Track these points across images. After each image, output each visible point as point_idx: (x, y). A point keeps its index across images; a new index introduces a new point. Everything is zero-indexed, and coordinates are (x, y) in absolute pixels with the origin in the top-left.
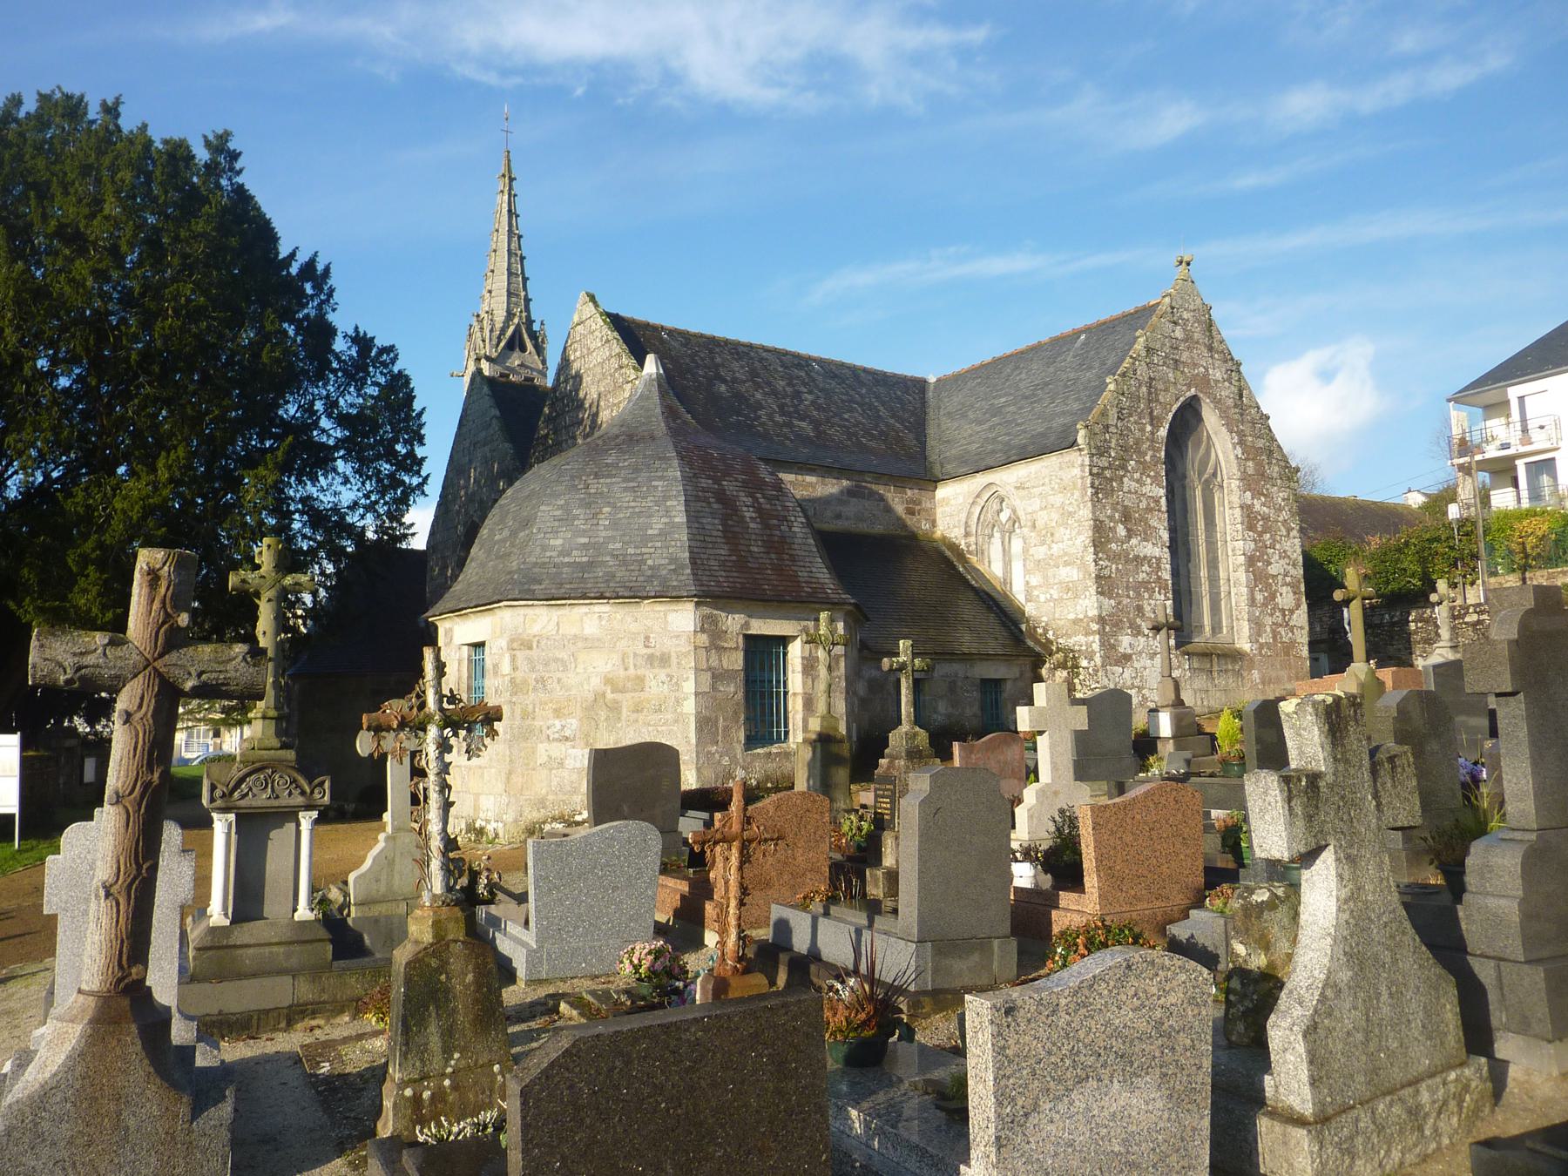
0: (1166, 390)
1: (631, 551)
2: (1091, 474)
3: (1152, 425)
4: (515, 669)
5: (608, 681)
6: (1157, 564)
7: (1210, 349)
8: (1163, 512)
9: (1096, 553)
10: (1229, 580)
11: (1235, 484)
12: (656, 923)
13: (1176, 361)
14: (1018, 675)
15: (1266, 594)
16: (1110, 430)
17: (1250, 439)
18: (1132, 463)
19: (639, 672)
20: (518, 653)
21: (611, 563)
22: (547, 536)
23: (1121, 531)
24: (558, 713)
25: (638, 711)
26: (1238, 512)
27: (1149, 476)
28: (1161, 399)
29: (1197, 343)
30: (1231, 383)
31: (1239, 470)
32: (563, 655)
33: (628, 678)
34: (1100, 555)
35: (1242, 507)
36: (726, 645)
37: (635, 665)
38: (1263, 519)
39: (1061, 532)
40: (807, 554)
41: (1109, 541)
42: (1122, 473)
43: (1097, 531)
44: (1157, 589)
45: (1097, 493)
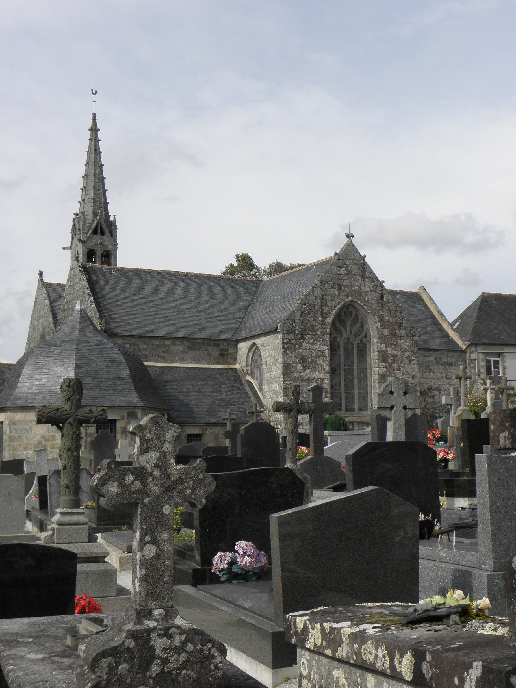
0: (332, 300)
1: (53, 388)
2: (283, 343)
3: (322, 317)
4: (10, 432)
5: (43, 437)
6: (321, 381)
7: (363, 277)
8: (326, 357)
9: (284, 378)
10: (372, 387)
11: (376, 340)
13: (340, 286)
16: (296, 321)
17: (387, 318)
18: (308, 336)
19: (54, 434)
20: (12, 427)
21: (46, 392)
22: (25, 381)
23: (300, 367)
24: (25, 449)
25: (53, 448)
26: (376, 354)
27: (319, 341)
28: (329, 304)
29: (355, 275)
30: (376, 292)
31: (378, 334)
32: (27, 427)
33: (50, 436)
34: (287, 379)
35: (379, 352)
37: (52, 431)
39: (274, 367)
41: (292, 372)
42: (302, 341)
43: (285, 368)
45: (286, 351)
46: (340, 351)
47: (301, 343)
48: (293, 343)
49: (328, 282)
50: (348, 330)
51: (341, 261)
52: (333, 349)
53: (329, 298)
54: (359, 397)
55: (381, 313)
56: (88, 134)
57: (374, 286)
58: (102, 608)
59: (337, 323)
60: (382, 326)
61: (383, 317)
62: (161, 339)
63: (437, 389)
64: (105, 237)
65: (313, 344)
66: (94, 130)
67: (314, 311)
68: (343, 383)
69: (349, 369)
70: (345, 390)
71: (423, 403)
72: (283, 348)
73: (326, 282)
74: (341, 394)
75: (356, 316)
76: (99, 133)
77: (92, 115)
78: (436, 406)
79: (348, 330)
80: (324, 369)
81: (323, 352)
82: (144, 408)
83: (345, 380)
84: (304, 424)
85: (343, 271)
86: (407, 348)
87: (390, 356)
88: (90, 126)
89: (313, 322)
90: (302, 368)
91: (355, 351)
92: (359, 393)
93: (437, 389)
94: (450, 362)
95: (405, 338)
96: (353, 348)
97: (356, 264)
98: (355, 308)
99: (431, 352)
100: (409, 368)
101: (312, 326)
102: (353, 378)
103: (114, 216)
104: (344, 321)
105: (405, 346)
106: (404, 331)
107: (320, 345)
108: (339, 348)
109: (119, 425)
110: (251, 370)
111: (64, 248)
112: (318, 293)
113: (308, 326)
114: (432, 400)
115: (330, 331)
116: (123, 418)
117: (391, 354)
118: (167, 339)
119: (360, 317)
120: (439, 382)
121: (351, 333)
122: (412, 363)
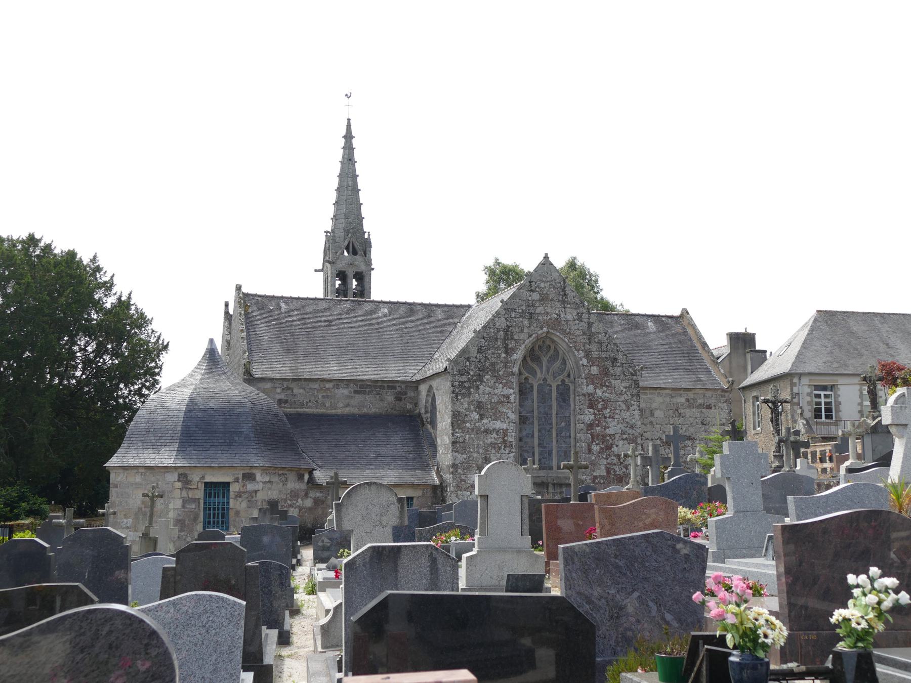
3: (506, 352)
7: (563, 302)
12: (788, 517)
14: (421, 494)
15: (602, 446)
17: (596, 353)
23: (475, 416)
27: (501, 383)
28: (516, 337)
29: (552, 300)
36: (190, 487)
38: (603, 401)
40: (207, 441)
41: (465, 422)
44: (503, 447)
45: (457, 396)
46: (533, 395)
48: (467, 386)
49: (515, 309)
50: (544, 368)
51: (533, 284)
52: (523, 392)
53: (517, 330)
56: (342, 142)
57: (578, 313)
58: (748, 599)
59: (528, 359)
60: (588, 362)
61: (591, 352)
62: (321, 381)
64: (357, 257)
66: (349, 137)
67: (496, 346)
68: (536, 434)
69: (545, 419)
70: (539, 444)
72: (453, 392)
73: (513, 310)
74: (534, 448)
75: (556, 349)
77: (347, 121)
79: (544, 368)
80: (508, 417)
81: (507, 397)
82: (263, 468)
83: (539, 431)
85: (536, 296)
86: (624, 390)
87: (601, 400)
88: (344, 133)
89: (493, 360)
90: (477, 417)
91: (554, 394)
92: (558, 447)
94: (708, 404)
95: (622, 377)
97: (554, 288)
98: (553, 341)
99: (681, 392)
100: (626, 415)
101: (493, 364)
102: (552, 428)
103: (369, 233)
104: (539, 357)
105: (622, 388)
106: (620, 369)
107: (503, 388)
108: (532, 391)
109: (234, 488)
110: (431, 418)
111: (316, 271)
112: (501, 323)
113: (488, 365)
115: (519, 370)
116: (237, 480)
117: (601, 398)
118: (328, 381)
119: (561, 352)
120: (692, 430)
121: (548, 373)
122: (631, 408)
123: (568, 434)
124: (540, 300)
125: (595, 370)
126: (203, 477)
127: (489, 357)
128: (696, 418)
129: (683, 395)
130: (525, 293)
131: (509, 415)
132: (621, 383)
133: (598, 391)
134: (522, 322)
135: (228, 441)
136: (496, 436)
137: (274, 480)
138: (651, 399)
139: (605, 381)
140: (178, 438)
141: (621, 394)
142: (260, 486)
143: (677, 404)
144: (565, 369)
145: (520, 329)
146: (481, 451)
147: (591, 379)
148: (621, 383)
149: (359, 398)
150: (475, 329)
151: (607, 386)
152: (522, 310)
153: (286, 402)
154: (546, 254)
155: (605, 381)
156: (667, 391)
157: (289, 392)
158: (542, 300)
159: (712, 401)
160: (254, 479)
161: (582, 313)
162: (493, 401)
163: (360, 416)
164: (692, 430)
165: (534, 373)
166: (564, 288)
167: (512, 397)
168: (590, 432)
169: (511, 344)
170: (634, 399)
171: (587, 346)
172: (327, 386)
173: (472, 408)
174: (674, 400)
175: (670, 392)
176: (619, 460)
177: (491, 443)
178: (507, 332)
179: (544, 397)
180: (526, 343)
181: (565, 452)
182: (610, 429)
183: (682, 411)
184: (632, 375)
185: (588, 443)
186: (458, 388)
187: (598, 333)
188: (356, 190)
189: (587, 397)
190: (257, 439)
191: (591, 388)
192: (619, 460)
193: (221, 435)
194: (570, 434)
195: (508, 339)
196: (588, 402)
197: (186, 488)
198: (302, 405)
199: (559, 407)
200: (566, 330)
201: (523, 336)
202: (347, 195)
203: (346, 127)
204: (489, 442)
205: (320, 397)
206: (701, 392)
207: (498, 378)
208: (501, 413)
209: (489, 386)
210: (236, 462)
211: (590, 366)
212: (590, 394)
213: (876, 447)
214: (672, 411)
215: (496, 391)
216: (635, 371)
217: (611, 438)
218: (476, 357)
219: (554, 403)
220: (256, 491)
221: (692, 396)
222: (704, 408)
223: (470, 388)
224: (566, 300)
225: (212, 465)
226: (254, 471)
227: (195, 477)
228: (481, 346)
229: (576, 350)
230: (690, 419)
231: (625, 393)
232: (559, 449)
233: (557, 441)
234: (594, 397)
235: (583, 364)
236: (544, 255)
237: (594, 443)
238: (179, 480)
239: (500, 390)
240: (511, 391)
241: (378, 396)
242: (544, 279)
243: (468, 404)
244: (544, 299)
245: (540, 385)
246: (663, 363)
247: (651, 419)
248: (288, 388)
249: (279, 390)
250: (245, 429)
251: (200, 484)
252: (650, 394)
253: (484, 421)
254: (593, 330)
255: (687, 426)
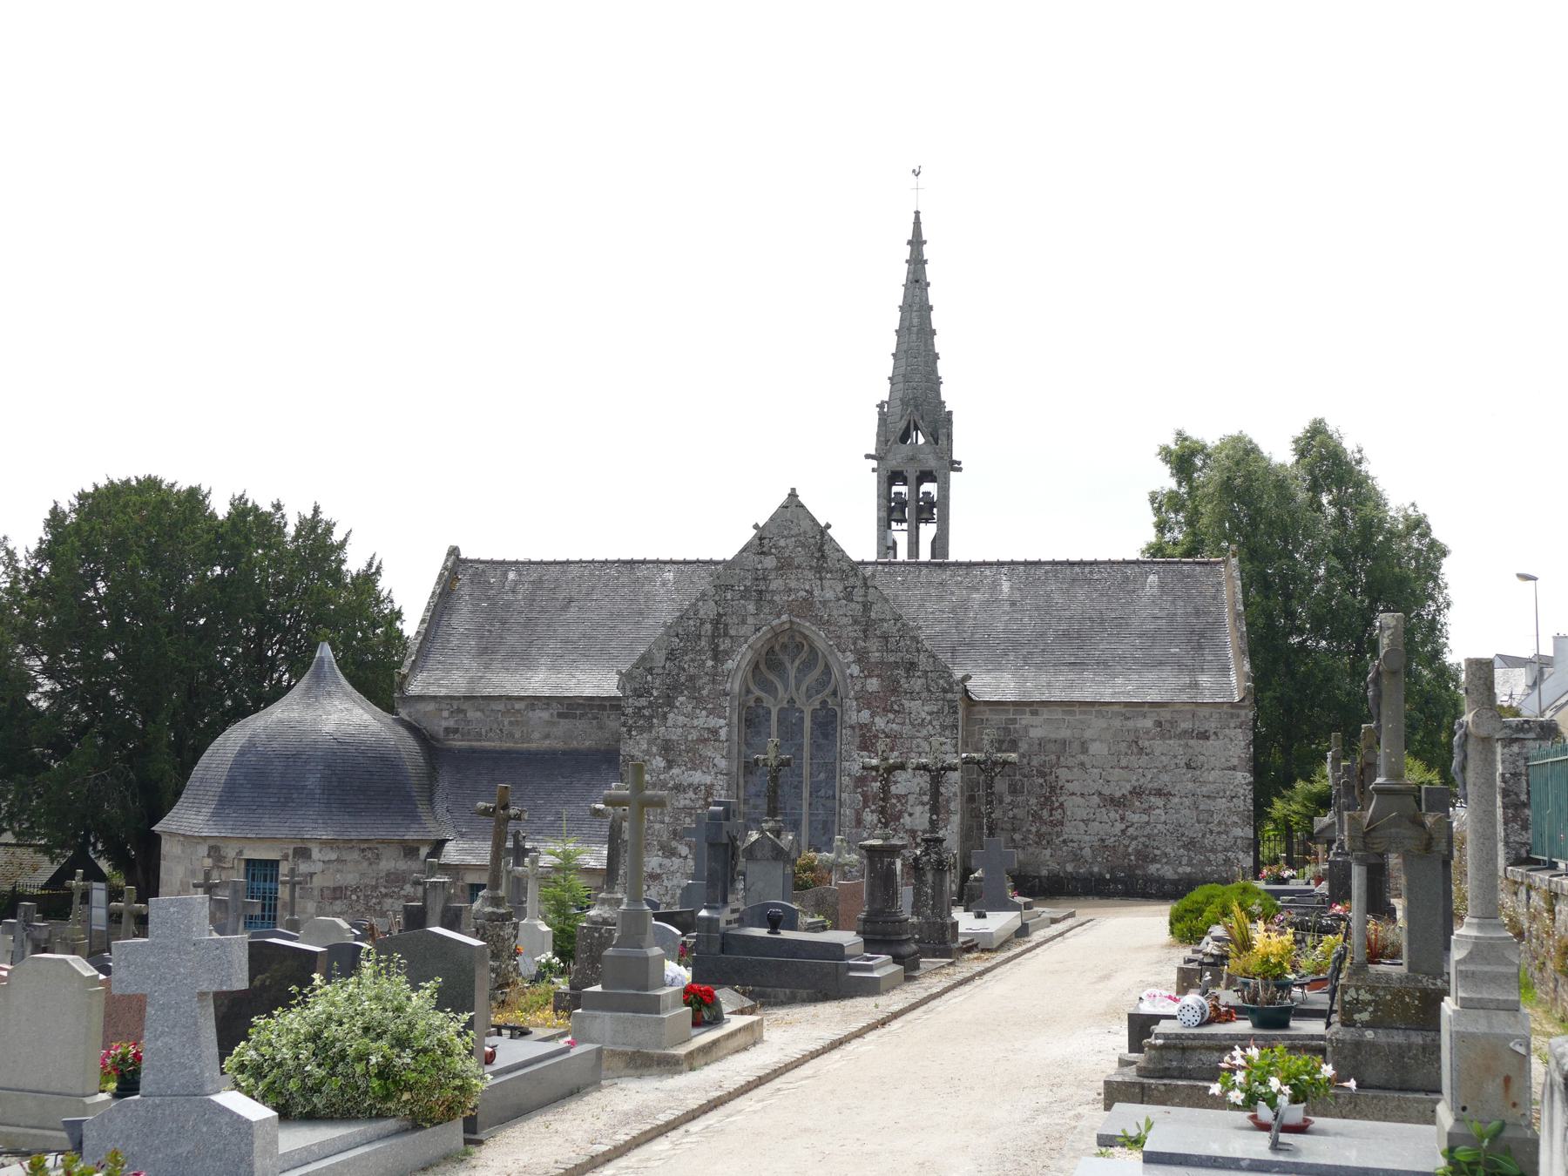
3: (715, 658)
7: (819, 570)
17: (877, 654)
23: (659, 762)
28: (732, 632)
30: (852, 600)
47: (666, 713)
48: (647, 714)
50: (792, 682)
52: (752, 720)
54: (811, 822)
55: (863, 644)
56: (906, 252)
57: (846, 588)
63: (1159, 793)
65: (691, 716)
66: (917, 242)
71: (1117, 824)
76: (925, 247)
77: (914, 215)
78: (1156, 831)
79: (792, 682)
81: (715, 732)
84: (664, 876)
85: (770, 562)
86: (929, 718)
87: (883, 736)
90: (663, 764)
91: (807, 723)
93: (1159, 793)
94: (1202, 730)
95: (924, 695)
96: (802, 719)
97: (803, 546)
98: (806, 637)
99: (1146, 709)
101: (692, 678)
102: (801, 782)
105: (923, 715)
107: (707, 717)
108: (768, 720)
109: (284, 868)
112: (708, 610)
113: (683, 679)
114: (1145, 818)
116: (286, 858)
117: (884, 732)
120: (1165, 778)
123: (831, 793)
124: (778, 569)
125: (873, 684)
126: (240, 852)
127: (686, 666)
128: (1175, 757)
129: (1148, 715)
130: (752, 557)
131: (716, 761)
132: (923, 705)
133: (877, 719)
134: (744, 606)
135: (282, 800)
136: (693, 796)
137: (348, 858)
138: (1082, 722)
139: (892, 702)
140: (218, 794)
141: (922, 724)
142: (318, 867)
143: (1136, 731)
144: (829, 682)
145: (740, 619)
146: (667, 819)
147: (865, 700)
148: (923, 705)
149: (565, 724)
150: (665, 622)
151: (896, 711)
152: (745, 586)
153: (456, 731)
154: (793, 490)
155: (892, 702)
156: (1116, 708)
157: (461, 716)
158: (781, 568)
159: (1211, 726)
160: (310, 857)
161: (853, 587)
162: (690, 738)
163: (564, 753)
164: (1165, 778)
165: (770, 689)
166: (822, 545)
167: (723, 733)
168: (859, 790)
169: (724, 644)
170: (947, 733)
171: (861, 643)
172: (517, 706)
173: (654, 749)
174: (1130, 724)
175: (1124, 710)
176: (914, 839)
177: (685, 807)
178: (717, 623)
179: (790, 731)
180: (750, 641)
181: (825, 823)
182: (898, 785)
183: (1147, 743)
184: (945, 691)
185: (856, 810)
186: (632, 718)
187: (882, 620)
188: (927, 333)
189: (857, 730)
190: (326, 797)
191: (865, 715)
192: (914, 839)
193: (275, 791)
194: (834, 792)
195: (719, 636)
196: (858, 740)
197: (218, 867)
198: (479, 737)
199: (816, 746)
200: (821, 617)
201: (745, 630)
202: (909, 343)
203: (912, 226)
204: (681, 806)
205: (506, 723)
206: (1187, 708)
207: (699, 701)
208: (703, 758)
209: (684, 715)
210: (284, 832)
211: (866, 677)
212: (862, 726)
213: (753, 884)
214: (1124, 744)
215: (696, 722)
216: (950, 685)
217: (899, 801)
218: (664, 667)
219: (807, 741)
220: (312, 875)
221: (1168, 717)
222: (1193, 738)
223: (652, 717)
224: (825, 565)
225: (249, 836)
226: (309, 845)
227: (230, 852)
228: (672, 650)
229: (839, 650)
230: (1163, 758)
231: (930, 722)
232: (813, 818)
233: (810, 804)
234: (869, 730)
235: (851, 675)
236: (789, 491)
237: (868, 810)
238: (209, 856)
239: (703, 720)
240: (722, 722)
241: (594, 722)
242: (785, 533)
243: (648, 744)
244: (785, 565)
245: (781, 710)
246: (1138, 654)
247: (1082, 758)
248: (459, 711)
249: (446, 714)
250: (312, 781)
251: (236, 861)
252: (1081, 713)
253: (673, 771)
254: (873, 615)
255: (1155, 771)
